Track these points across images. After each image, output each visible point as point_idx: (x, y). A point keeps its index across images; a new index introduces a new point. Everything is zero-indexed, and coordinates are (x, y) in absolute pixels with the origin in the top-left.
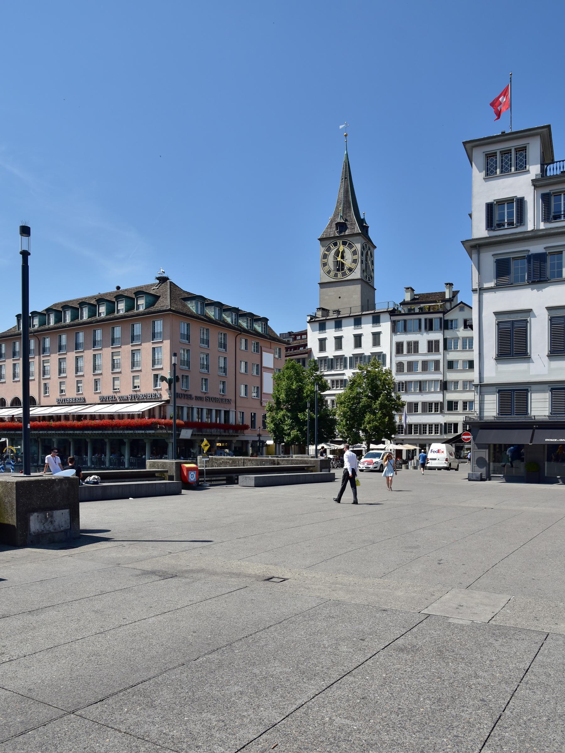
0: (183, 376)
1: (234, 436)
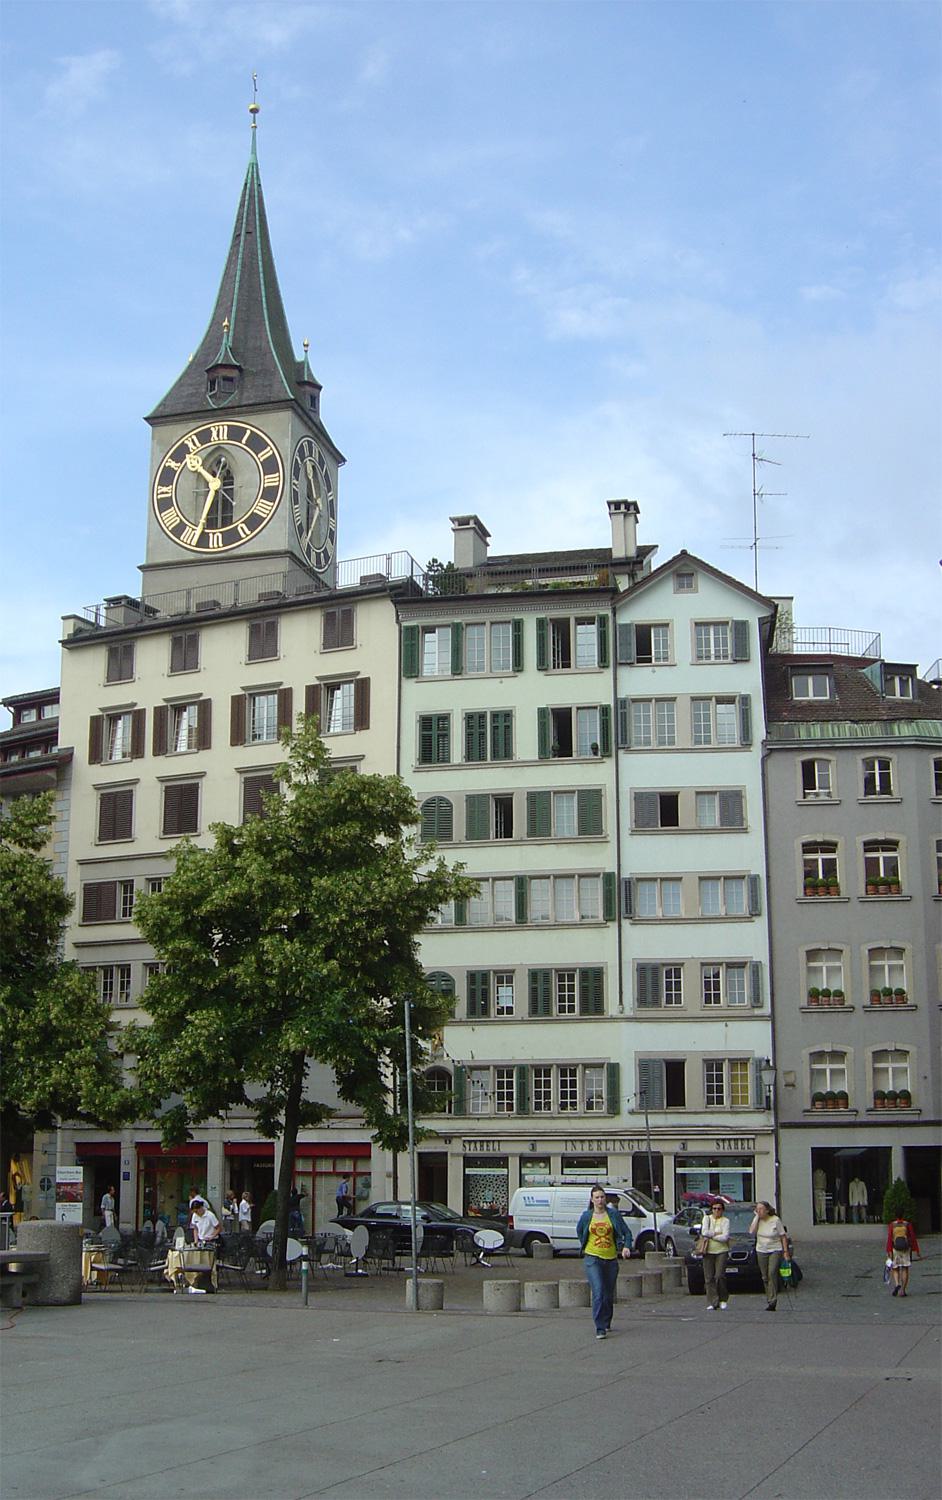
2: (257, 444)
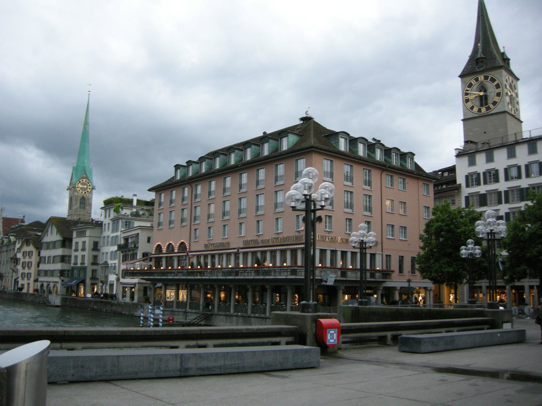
0: (326, 216)
1: (381, 282)
2: (493, 80)
